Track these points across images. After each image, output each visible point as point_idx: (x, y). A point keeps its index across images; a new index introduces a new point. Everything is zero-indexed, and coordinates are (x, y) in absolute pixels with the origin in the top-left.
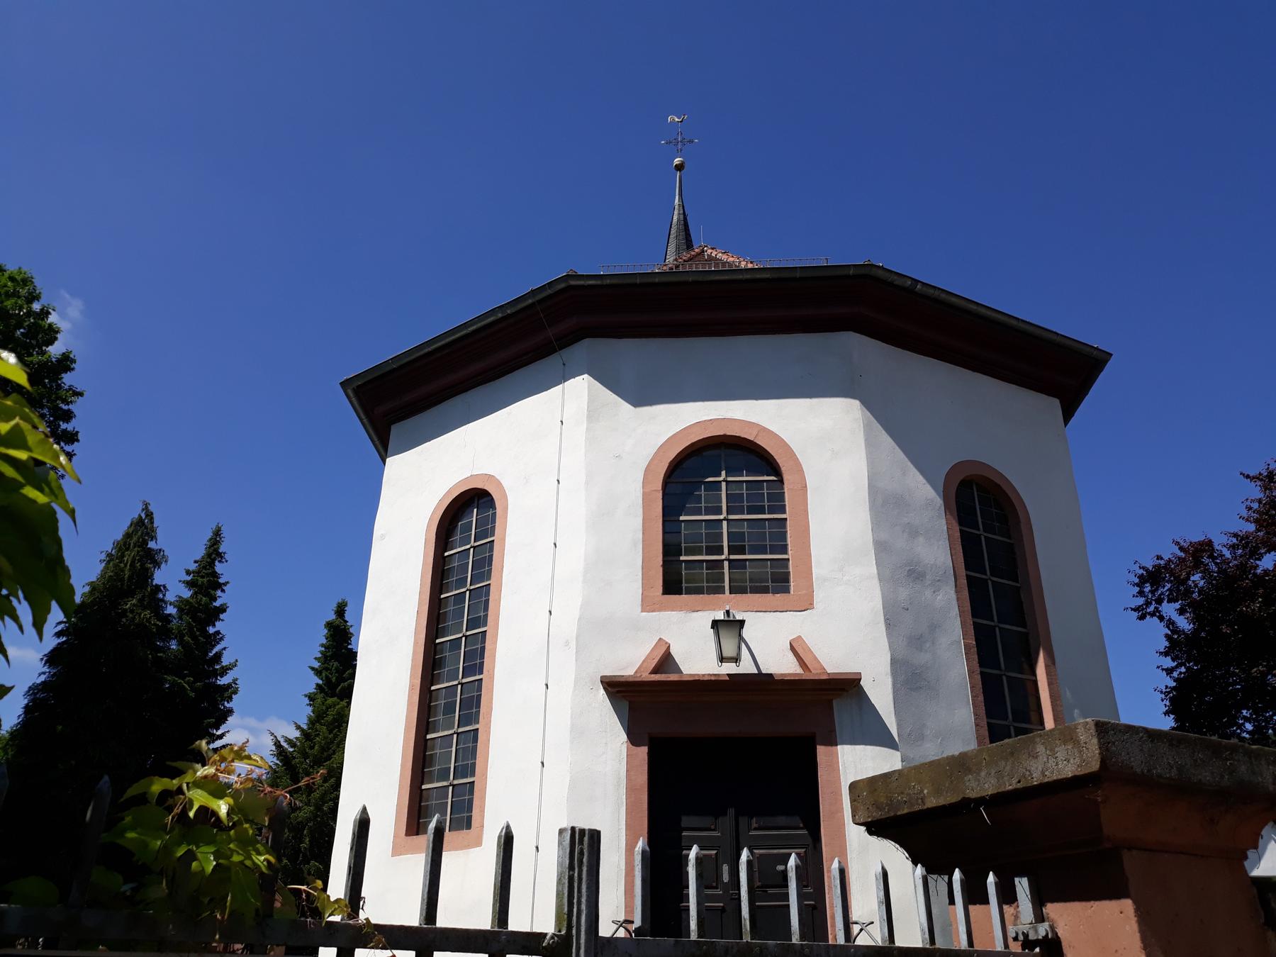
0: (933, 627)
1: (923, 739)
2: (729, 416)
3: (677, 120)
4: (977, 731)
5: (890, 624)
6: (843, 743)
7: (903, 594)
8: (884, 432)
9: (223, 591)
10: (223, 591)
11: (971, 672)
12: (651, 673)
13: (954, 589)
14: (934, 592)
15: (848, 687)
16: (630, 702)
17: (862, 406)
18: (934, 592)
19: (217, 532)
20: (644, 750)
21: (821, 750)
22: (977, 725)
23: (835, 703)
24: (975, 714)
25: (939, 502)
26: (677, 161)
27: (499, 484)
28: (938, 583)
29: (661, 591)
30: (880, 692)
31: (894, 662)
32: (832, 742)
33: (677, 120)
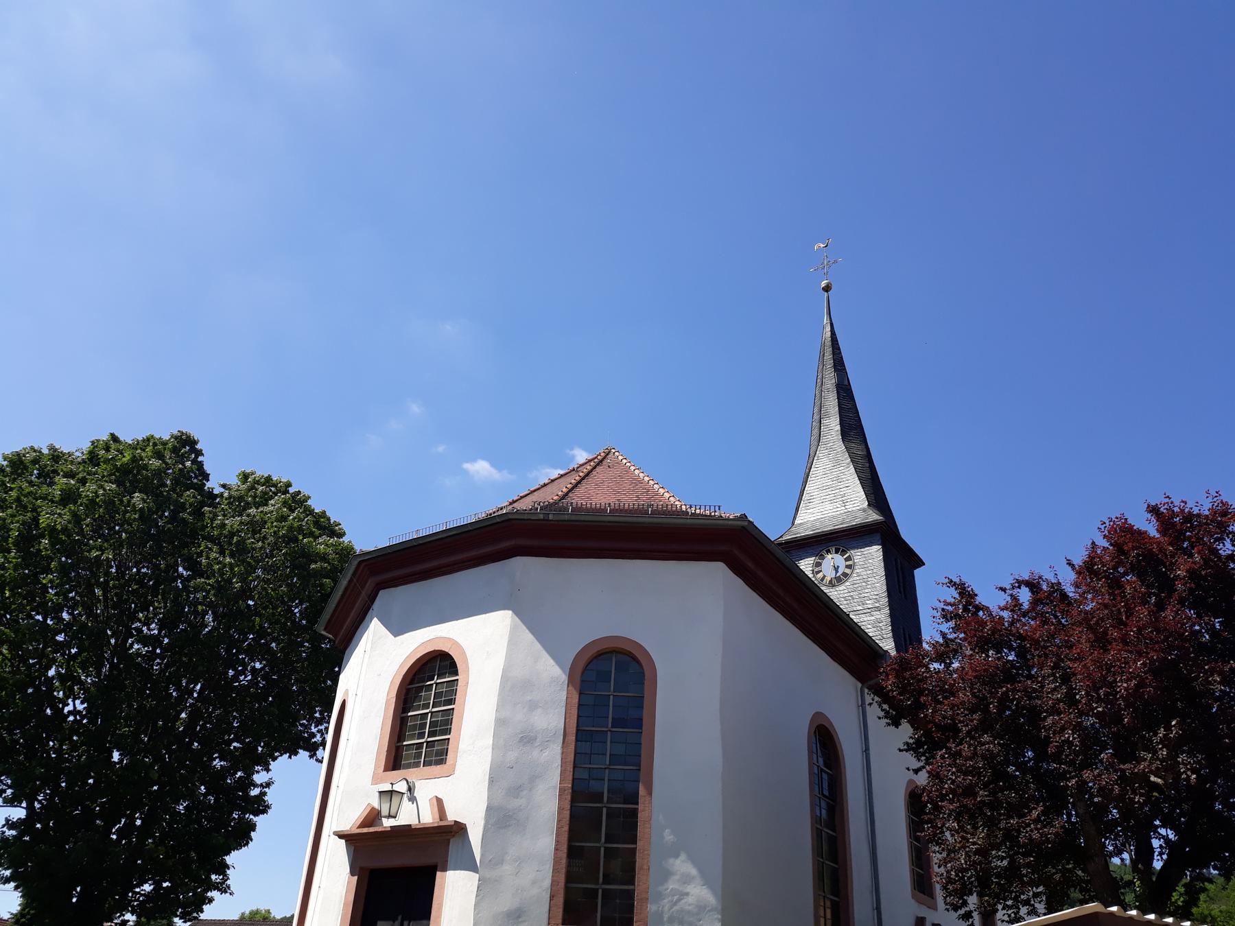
0: (533, 779)
1: (502, 864)
2: (439, 635)
3: (822, 246)
4: (555, 854)
5: (492, 781)
6: (456, 868)
7: (512, 756)
8: (527, 631)
9: (1134, 526)
10: (1134, 526)
11: (560, 809)
12: (358, 828)
13: (561, 745)
14: (541, 751)
15: (459, 830)
16: (355, 847)
17: (514, 615)
18: (541, 751)
19: (344, 700)
20: (356, 878)
21: (438, 874)
22: (556, 849)
23: (451, 840)
24: (557, 841)
25: (564, 678)
26: (823, 284)
27: (463, 653)
28: (547, 743)
29: (383, 770)
30: (475, 836)
31: (489, 809)
32: (445, 869)
33: (822, 246)
